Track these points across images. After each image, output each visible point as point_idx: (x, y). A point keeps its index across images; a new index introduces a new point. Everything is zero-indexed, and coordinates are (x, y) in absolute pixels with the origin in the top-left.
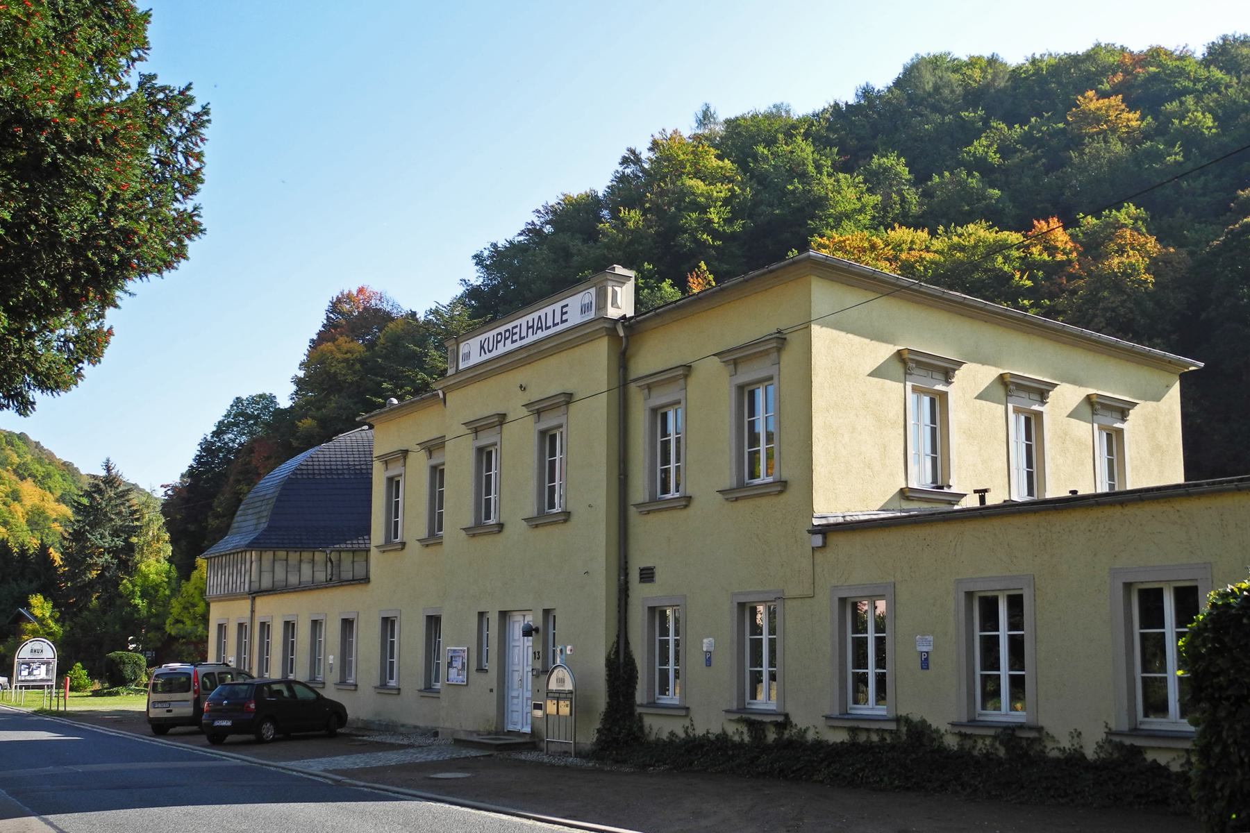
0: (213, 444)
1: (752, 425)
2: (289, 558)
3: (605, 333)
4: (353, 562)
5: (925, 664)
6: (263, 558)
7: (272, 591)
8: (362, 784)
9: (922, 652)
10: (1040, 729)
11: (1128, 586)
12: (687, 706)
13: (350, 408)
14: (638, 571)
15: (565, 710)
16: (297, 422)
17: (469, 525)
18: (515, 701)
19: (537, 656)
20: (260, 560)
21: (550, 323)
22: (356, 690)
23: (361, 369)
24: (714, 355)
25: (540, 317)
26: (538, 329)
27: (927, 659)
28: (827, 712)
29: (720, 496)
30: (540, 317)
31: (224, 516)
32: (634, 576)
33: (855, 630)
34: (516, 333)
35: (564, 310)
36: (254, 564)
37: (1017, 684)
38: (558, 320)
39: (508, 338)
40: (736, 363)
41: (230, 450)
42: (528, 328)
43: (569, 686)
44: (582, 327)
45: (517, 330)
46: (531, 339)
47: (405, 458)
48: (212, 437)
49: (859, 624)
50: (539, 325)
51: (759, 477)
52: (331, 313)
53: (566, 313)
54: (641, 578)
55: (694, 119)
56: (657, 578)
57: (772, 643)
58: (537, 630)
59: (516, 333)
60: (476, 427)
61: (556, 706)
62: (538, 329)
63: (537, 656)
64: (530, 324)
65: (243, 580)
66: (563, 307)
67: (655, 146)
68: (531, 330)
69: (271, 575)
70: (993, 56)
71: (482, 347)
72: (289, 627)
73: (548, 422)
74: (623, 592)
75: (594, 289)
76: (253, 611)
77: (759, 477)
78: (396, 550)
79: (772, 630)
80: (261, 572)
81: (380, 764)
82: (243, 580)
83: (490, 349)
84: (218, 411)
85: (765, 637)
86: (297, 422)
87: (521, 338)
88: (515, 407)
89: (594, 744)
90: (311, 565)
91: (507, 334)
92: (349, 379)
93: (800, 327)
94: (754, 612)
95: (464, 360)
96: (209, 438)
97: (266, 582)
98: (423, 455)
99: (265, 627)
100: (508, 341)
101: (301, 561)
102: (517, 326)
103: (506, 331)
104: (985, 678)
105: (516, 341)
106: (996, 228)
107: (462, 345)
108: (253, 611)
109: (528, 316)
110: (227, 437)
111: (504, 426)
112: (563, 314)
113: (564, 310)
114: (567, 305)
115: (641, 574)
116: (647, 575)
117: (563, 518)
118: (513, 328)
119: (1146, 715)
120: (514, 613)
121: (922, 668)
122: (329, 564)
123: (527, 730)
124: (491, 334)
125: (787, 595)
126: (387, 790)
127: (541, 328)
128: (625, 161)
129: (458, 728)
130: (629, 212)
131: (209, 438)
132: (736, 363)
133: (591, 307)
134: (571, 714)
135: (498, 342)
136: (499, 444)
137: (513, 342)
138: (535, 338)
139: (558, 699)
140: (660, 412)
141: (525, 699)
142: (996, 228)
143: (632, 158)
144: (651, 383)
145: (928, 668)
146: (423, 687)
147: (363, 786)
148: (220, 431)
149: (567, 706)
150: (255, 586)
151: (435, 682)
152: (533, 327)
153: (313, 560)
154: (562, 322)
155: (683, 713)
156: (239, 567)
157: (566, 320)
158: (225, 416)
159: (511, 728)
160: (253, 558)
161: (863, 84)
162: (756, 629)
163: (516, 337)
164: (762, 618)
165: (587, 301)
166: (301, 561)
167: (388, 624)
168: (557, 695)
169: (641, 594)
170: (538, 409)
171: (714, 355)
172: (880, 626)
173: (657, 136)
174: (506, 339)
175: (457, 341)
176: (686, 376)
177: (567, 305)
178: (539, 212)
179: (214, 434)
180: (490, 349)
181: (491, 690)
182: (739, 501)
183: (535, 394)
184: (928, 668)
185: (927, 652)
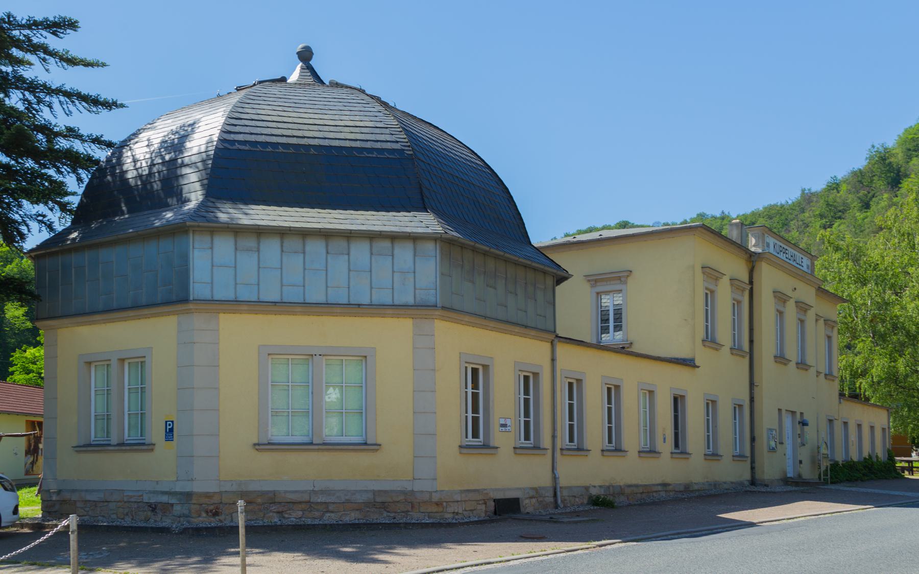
99: (575, 387)
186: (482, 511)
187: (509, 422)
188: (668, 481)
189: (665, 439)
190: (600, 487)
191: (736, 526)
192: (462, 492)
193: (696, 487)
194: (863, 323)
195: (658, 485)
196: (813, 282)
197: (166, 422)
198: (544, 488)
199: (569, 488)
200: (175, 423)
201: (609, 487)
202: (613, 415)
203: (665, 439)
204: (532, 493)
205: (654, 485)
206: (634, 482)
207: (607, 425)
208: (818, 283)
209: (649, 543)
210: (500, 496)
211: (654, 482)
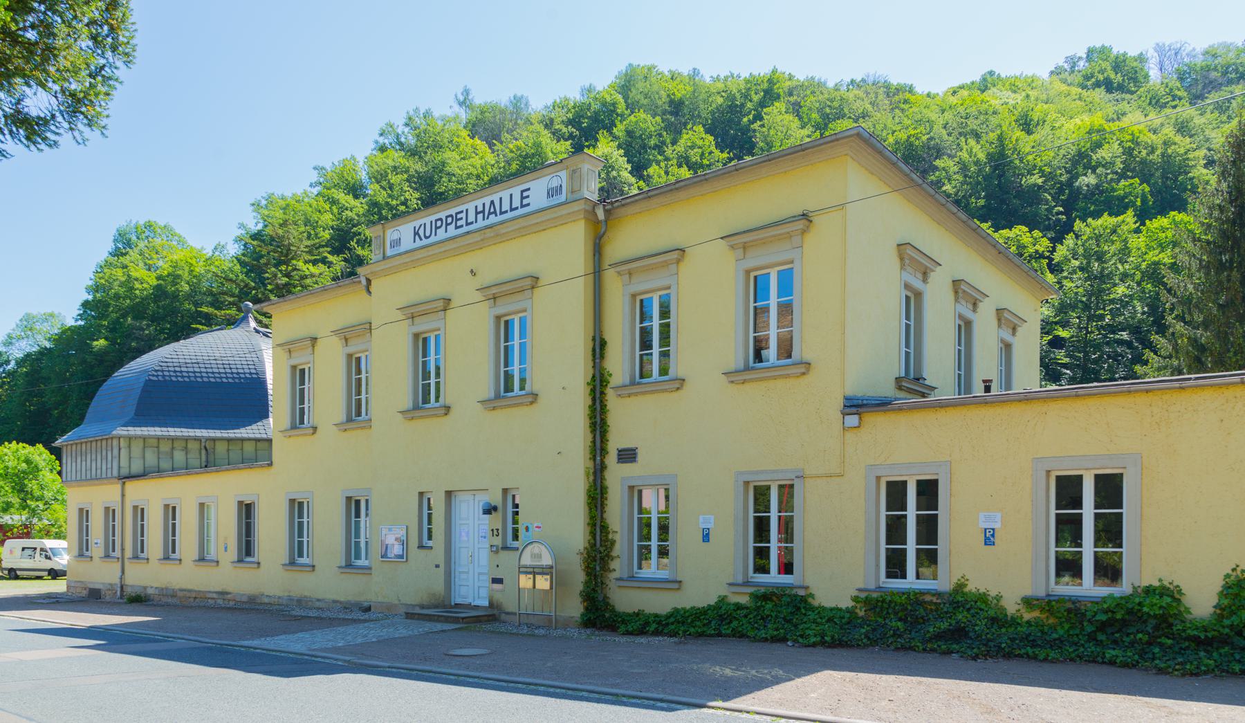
1: (425, 363)
2: (161, 446)
3: (582, 216)
4: (228, 450)
5: (706, 537)
6: (132, 444)
7: (142, 475)
8: (387, 664)
10: (807, 588)
11: (747, 483)
12: (679, 579)
14: (616, 452)
15: (543, 583)
17: (732, 367)
18: (464, 576)
19: (495, 532)
20: (129, 447)
21: (506, 207)
22: (313, 570)
24: (722, 238)
25: (492, 202)
26: (490, 213)
27: (708, 534)
29: (335, 427)
30: (492, 202)
32: (611, 459)
34: (462, 219)
35: (525, 194)
36: (123, 451)
37: (663, 552)
38: (516, 203)
39: (451, 223)
40: (745, 247)
42: (477, 213)
43: (547, 560)
44: (556, 209)
45: (463, 215)
46: (481, 223)
47: (313, 346)
50: (492, 210)
51: (429, 403)
53: (528, 197)
54: (619, 459)
56: (639, 458)
58: (495, 508)
59: (462, 219)
60: (413, 312)
61: (531, 581)
62: (490, 213)
63: (495, 532)
64: (480, 208)
65: (109, 466)
66: (522, 192)
68: (480, 216)
69: (142, 462)
71: (416, 233)
72: (171, 512)
73: (766, 258)
74: (598, 472)
75: (564, 172)
76: (123, 495)
77: (429, 403)
78: (305, 435)
80: (130, 458)
81: (296, 635)
82: (109, 466)
83: (427, 234)
87: (467, 224)
88: (465, 291)
89: (582, 615)
90: (184, 452)
91: (439, 223)
93: (830, 210)
95: (392, 246)
97: (137, 467)
98: (336, 342)
99: (139, 513)
100: (451, 228)
101: (173, 448)
102: (462, 212)
103: (447, 217)
104: (640, 547)
105: (462, 226)
107: (389, 232)
108: (123, 495)
109: (415, 222)
111: (535, 290)
112: (523, 198)
113: (525, 194)
114: (529, 189)
115: (619, 455)
116: (627, 456)
117: (530, 400)
118: (457, 214)
119: (755, 572)
120: (456, 493)
122: (203, 452)
123: (486, 603)
124: (427, 220)
125: (807, 472)
127: (495, 212)
128: (387, 124)
129: (396, 602)
132: (745, 247)
133: (561, 190)
134: (551, 588)
135: (437, 228)
136: (442, 329)
137: (457, 227)
138: (487, 222)
139: (534, 574)
140: (752, 275)
141: (476, 575)
144: (630, 266)
145: (708, 541)
146: (344, 564)
147: (389, 667)
149: (546, 579)
150: (124, 472)
151: (299, 557)
152: (483, 212)
153: (186, 448)
154: (523, 206)
155: (676, 586)
156: (104, 453)
157: (528, 205)
159: (459, 601)
160: (122, 445)
163: (462, 222)
165: (555, 183)
166: (173, 448)
167: (297, 508)
168: (531, 570)
169: (617, 475)
170: (494, 293)
171: (722, 238)
174: (447, 224)
175: (383, 228)
176: (678, 261)
177: (529, 189)
180: (427, 234)
181: (437, 566)
182: (291, 438)
183: (487, 277)
186: (85, 593)
187: (99, 541)
188: (229, 589)
189: (226, 548)
190: (156, 588)
191: (662, 700)
192: (76, 582)
193: (266, 600)
194: (1237, 69)
195: (216, 592)
196: (543, 222)
197: (986, 529)
198: (115, 584)
199: (132, 586)
200: (996, 531)
201: (162, 589)
202: (171, 530)
203: (226, 548)
204: (109, 587)
205: (210, 592)
206: (189, 587)
207: (116, 538)
208: (576, 209)
209: (637, 710)
210: (92, 586)
211: (212, 590)
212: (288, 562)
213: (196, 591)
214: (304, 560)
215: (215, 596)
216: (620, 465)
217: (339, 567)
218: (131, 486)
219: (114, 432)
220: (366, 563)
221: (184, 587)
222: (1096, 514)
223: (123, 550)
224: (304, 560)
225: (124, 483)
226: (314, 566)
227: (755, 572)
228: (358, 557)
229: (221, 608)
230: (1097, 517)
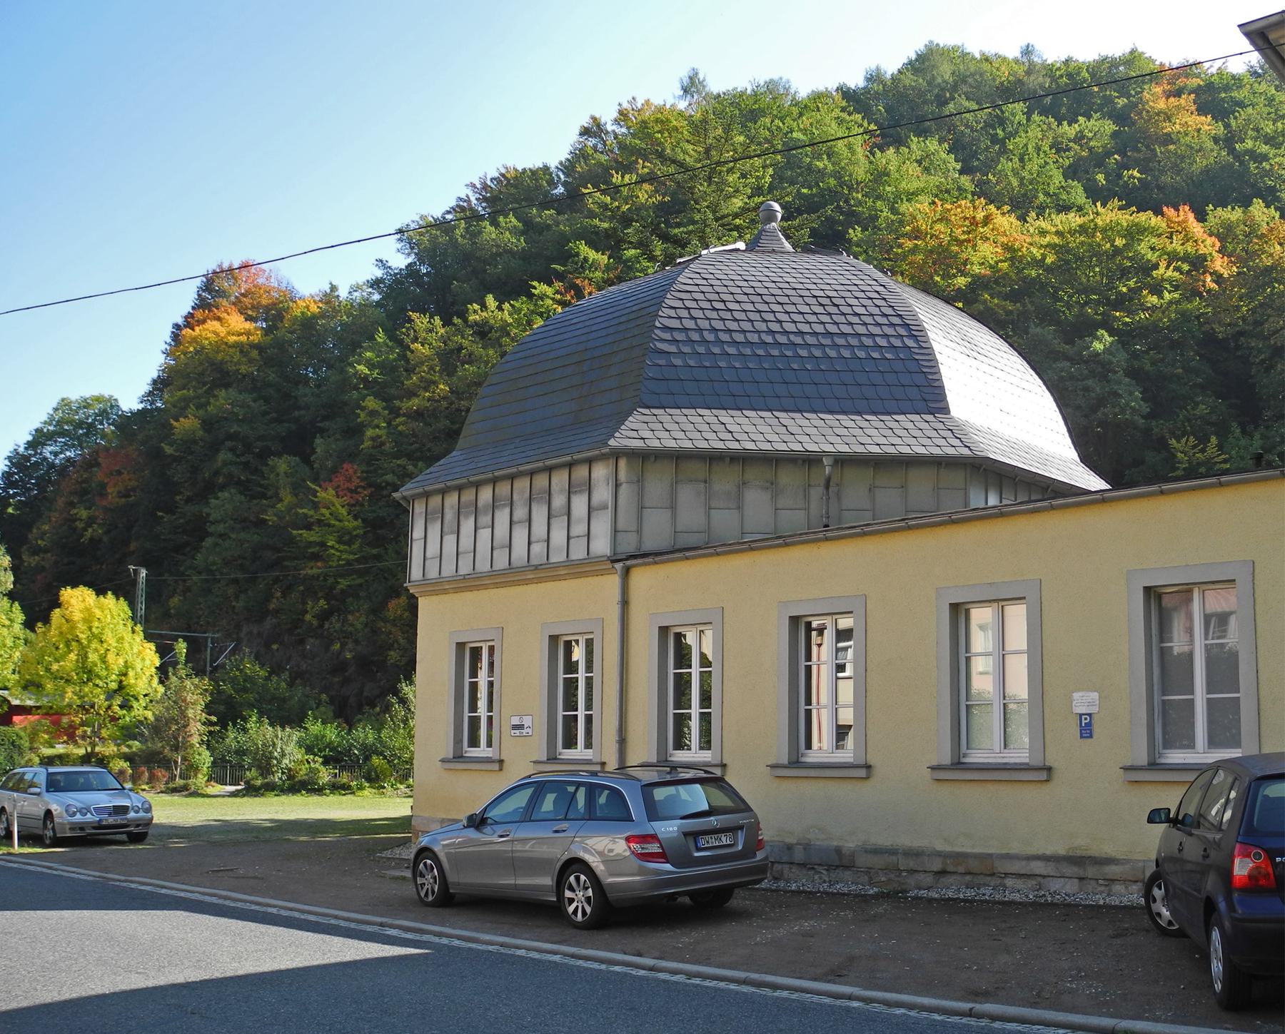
0: (27, 458)
9: (1081, 715)
13: (249, 407)
16: (172, 421)
23: (258, 357)
27: (1089, 725)
28: (772, 761)
31: (46, 551)
33: (678, 665)
41: (52, 465)
48: (26, 448)
49: (683, 656)
52: (204, 291)
55: (679, 86)
57: (589, 682)
67: (623, 116)
70: (1028, 46)
76: (625, 603)
79: (589, 668)
84: (37, 415)
85: (581, 675)
86: (172, 421)
92: (243, 369)
94: (568, 647)
96: (21, 450)
106: (1134, 208)
108: (625, 603)
110: (47, 451)
121: (1082, 737)
126: (336, 917)
128: (585, 132)
130: (623, 177)
131: (21, 450)
142: (1134, 208)
143: (593, 130)
145: (1091, 737)
148: (39, 439)
150: (628, 544)
155: (1043, 775)
158: (45, 423)
161: (874, 67)
162: (571, 667)
164: (578, 654)
172: (705, 661)
173: (625, 105)
178: (473, 186)
179: (30, 445)
184: (1091, 737)
185: (1090, 715)
187: (527, 721)
205: (1009, 857)
212: (451, 756)
213: (939, 854)
214: (482, 751)
215: (1038, 868)
216: (1142, 589)
217: (443, 761)
218: (643, 578)
219: (612, 442)
220: (588, 754)
221: (884, 840)
222: (701, 713)
223: (622, 742)
224: (482, 751)
225: (627, 571)
226: (1049, 769)
227: (563, 748)
228: (474, 742)
229: (1068, 910)
230: (1191, 691)
